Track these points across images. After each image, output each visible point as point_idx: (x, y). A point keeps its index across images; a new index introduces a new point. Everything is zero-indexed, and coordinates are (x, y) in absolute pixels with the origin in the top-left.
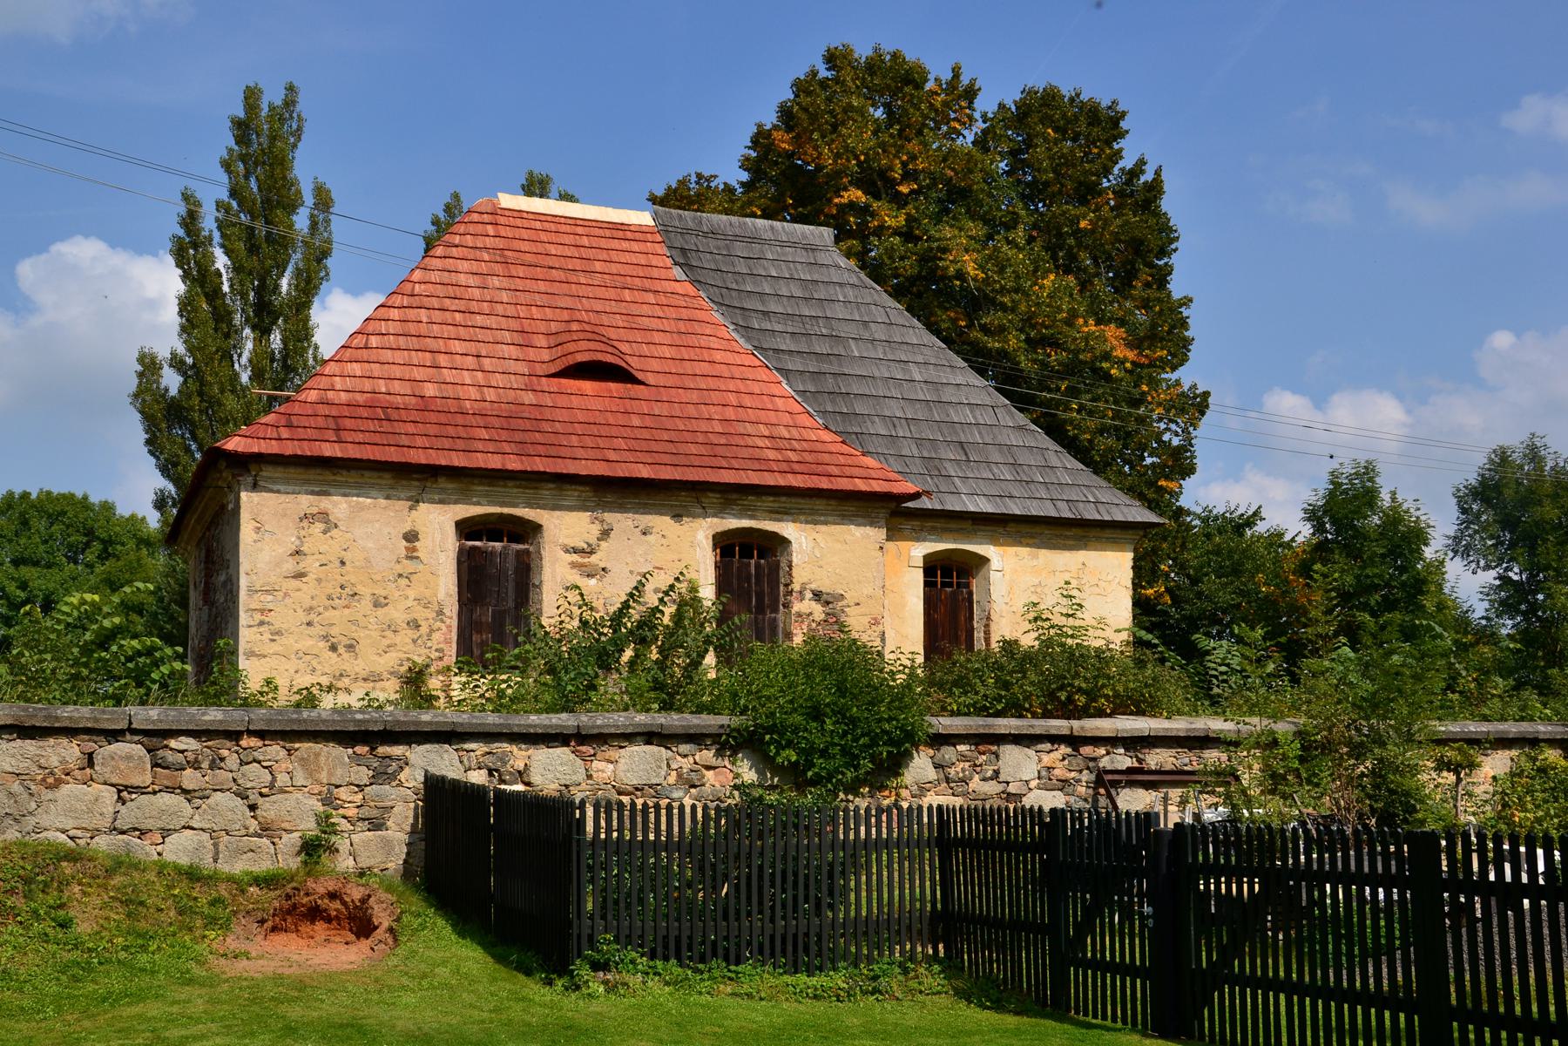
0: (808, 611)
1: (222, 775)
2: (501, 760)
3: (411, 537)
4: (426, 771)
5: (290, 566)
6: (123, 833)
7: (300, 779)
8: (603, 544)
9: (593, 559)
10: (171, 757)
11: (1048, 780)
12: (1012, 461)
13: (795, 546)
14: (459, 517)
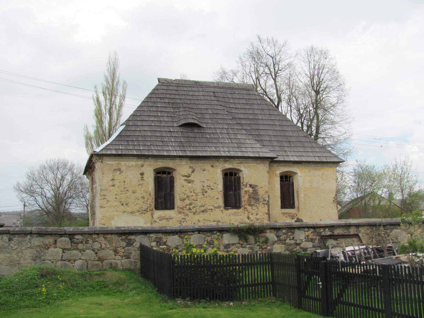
0: (248, 190)
1: (89, 245)
2: (160, 239)
3: (142, 174)
4: (140, 243)
5: (111, 183)
6: (64, 261)
7: (108, 246)
8: (193, 174)
9: (190, 178)
10: (75, 241)
11: (308, 239)
12: (303, 146)
13: (244, 172)
14: (156, 168)
